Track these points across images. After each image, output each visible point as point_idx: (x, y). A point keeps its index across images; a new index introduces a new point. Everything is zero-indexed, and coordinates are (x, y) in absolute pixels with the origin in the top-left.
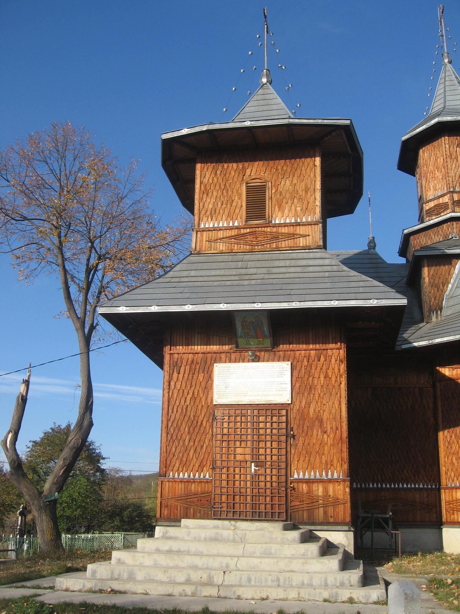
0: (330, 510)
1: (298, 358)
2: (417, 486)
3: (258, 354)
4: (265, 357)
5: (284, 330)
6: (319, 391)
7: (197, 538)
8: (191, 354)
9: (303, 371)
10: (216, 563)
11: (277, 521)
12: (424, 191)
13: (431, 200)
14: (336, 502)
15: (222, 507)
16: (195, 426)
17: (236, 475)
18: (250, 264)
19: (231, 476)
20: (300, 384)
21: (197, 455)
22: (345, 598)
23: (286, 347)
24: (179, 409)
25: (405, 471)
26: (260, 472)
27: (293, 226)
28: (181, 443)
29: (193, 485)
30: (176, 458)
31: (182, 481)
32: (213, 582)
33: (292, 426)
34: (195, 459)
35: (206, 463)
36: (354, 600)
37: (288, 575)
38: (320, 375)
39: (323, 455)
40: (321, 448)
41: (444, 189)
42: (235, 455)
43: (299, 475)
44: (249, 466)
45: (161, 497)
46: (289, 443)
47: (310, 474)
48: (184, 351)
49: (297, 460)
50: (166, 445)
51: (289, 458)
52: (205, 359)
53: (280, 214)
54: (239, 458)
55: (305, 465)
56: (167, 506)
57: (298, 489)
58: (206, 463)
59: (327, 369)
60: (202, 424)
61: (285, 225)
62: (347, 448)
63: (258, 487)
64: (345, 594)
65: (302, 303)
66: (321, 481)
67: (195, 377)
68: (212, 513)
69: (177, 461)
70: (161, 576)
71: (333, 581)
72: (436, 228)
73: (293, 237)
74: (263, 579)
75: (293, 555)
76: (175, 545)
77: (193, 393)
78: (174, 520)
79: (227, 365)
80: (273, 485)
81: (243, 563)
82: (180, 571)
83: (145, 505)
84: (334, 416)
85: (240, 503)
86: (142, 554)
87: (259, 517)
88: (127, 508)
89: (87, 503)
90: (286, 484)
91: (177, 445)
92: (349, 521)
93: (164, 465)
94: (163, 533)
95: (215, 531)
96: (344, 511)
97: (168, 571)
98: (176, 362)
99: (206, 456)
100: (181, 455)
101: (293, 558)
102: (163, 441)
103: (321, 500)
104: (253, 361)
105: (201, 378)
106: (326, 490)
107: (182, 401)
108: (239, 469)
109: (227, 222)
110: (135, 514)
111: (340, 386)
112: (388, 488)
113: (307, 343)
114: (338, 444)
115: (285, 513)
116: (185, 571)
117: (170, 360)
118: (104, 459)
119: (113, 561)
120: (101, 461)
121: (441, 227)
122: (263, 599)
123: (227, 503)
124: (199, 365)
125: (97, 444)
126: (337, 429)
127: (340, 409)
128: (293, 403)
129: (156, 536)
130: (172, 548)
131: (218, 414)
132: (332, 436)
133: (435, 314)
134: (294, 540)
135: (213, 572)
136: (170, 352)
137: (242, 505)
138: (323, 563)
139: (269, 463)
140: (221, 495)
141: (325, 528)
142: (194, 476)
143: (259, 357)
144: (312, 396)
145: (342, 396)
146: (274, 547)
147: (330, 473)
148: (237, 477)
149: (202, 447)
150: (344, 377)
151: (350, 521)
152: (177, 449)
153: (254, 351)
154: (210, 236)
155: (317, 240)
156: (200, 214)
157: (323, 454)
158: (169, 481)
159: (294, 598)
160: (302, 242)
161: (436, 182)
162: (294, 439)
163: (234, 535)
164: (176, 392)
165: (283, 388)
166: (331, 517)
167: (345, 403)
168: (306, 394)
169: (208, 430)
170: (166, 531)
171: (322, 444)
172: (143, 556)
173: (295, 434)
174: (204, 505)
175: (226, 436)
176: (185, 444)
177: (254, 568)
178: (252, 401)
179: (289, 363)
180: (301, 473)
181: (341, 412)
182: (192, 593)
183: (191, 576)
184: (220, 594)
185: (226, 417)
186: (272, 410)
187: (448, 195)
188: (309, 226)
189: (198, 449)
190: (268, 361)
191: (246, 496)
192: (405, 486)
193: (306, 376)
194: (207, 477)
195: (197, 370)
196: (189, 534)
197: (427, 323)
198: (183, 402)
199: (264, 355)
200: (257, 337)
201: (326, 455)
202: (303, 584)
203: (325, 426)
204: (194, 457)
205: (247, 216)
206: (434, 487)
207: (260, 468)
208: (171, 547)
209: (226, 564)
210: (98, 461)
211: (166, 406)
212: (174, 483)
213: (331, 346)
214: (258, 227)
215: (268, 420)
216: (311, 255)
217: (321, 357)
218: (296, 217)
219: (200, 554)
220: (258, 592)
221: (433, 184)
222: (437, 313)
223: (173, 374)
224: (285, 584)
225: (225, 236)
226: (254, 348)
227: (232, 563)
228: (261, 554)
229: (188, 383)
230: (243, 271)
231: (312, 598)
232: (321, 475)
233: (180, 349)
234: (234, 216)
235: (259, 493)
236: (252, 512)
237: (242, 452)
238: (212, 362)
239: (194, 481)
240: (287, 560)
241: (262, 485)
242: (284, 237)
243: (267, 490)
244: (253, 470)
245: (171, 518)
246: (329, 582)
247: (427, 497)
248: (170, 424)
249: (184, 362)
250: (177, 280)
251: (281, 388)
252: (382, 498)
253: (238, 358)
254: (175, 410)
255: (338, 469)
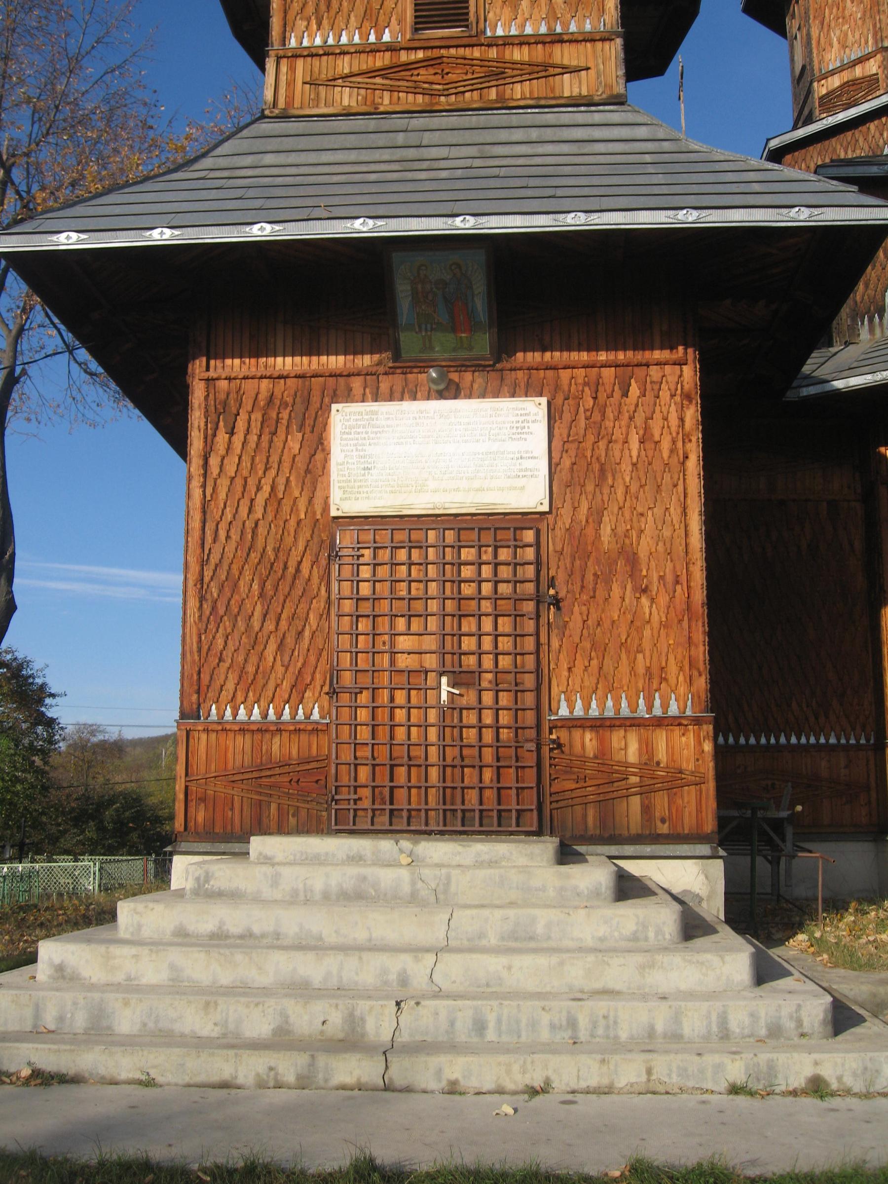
0: (661, 803)
1: (566, 388)
2: (822, 740)
3: (454, 376)
4: (476, 386)
5: (534, 302)
6: (628, 479)
7: (302, 894)
8: (265, 381)
9: (582, 423)
10: (366, 971)
11: (512, 833)
12: (815, 51)
13: (833, 73)
14: (675, 780)
15: (360, 799)
16: (278, 577)
17: (398, 711)
18: (427, 138)
19: (383, 713)
20: (575, 461)
21: (286, 659)
22: (798, 1081)
23: (533, 357)
24: (233, 531)
25: (794, 705)
26: (464, 702)
27: (544, 43)
28: (241, 625)
29: (277, 740)
30: (227, 665)
31: (244, 729)
32: (363, 1035)
33: (552, 573)
34: (280, 669)
35: (313, 679)
36: (827, 1084)
37: (602, 1006)
38: (627, 434)
39: (638, 652)
40: (634, 633)
41: (867, 42)
42: (393, 654)
43: (571, 709)
44: (434, 685)
45: (187, 775)
46: (543, 620)
47: (602, 706)
48: (245, 371)
49: (566, 666)
50: (199, 630)
51: (544, 662)
52: (306, 393)
53: (507, 12)
54: (403, 662)
55: (590, 682)
56: (203, 799)
57: (571, 746)
58: (313, 679)
59: (647, 419)
60: (298, 570)
61: (522, 39)
62: (704, 632)
63: (458, 743)
64: (797, 1068)
65: (595, 216)
66: (633, 723)
67: (278, 441)
68: (329, 816)
69: (230, 676)
70: (193, 1020)
71: (747, 1021)
72: (849, 134)
73: (543, 74)
74: (523, 1024)
75: (602, 940)
76: (233, 918)
77: (273, 488)
78: (228, 836)
79: (368, 409)
80: (501, 736)
81: (453, 970)
82: (257, 1005)
83: (150, 795)
84: (668, 545)
85: (409, 788)
86: (134, 950)
87: (463, 825)
88: (111, 801)
89: (17, 794)
90: (539, 733)
91: (229, 630)
92: (712, 832)
93: (192, 685)
94: (198, 879)
95: (353, 871)
96: (699, 805)
97: (216, 1003)
98: (225, 404)
99: (312, 659)
100: (241, 658)
101: (602, 950)
102: (190, 620)
103: (634, 774)
104: (441, 395)
105: (294, 445)
106: (647, 748)
107: (241, 508)
108: (404, 692)
109: (360, 34)
110: (127, 814)
111: (683, 463)
112: (753, 746)
113: (591, 347)
114: (680, 621)
115: (535, 813)
116: (271, 1002)
117: (207, 397)
118: (53, 696)
119: (42, 969)
120: (48, 701)
121: (863, 129)
122: (533, 1092)
123: (374, 788)
124: (289, 408)
125: (37, 665)
126: (677, 582)
127: (686, 526)
128: (554, 511)
129: (175, 884)
130: (225, 928)
131: (344, 540)
132: (663, 600)
133: (866, 322)
134: (596, 894)
135: (363, 1006)
136: (206, 375)
137: (413, 791)
138: (702, 963)
139: (489, 676)
140: (356, 765)
141: (648, 849)
142: (279, 715)
143: (458, 385)
144: (606, 491)
145: (689, 491)
146: (543, 919)
147: (657, 702)
148: (400, 715)
149: (300, 633)
150: (694, 439)
151: (716, 829)
152: (230, 642)
153: (444, 370)
154: (316, 70)
155: (609, 81)
156: (285, 12)
157: (640, 650)
158: (207, 731)
159: (632, 1085)
160: (569, 86)
161: (846, 27)
162: (559, 609)
163: (413, 883)
164: (224, 483)
165: (526, 470)
166: (663, 821)
167: (697, 510)
168: (590, 487)
169: (315, 587)
170: (207, 873)
171: (636, 623)
172: (134, 956)
173: (562, 594)
174: (305, 794)
175: (369, 604)
176: (252, 627)
177: (488, 985)
178: (447, 505)
179: (544, 400)
180: (579, 704)
181: (686, 535)
182: (299, 1077)
183: (292, 1020)
184: (391, 1079)
185: (366, 552)
186: (496, 529)
187: (879, 56)
188: (588, 45)
189: (290, 640)
190: (483, 396)
191: (427, 766)
192: (794, 740)
193: (591, 438)
194: (316, 716)
195: (285, 422)
196: (275, 882)
197: (847, 344)
198: (244, 511)
199: (473, 381)
200: (454, 330)
201: (648, 653)
202: (651, 1033)
203: (644, 573)
204: (279, 662)
205: (416, 17)
206: (863, 741)
207: (463, 691)
208: (222, 923)
209: (399, 975)
210: (40, 701)
211: (196, 524)
212: (222, 736)
213: (657, 355)
214: (449, 47)
215: (484, 558)
216: (597, 118)
217: (630, 385)
218: (552, 22)
219: (313, 946)
220: (516, 1068)
221: (838, 32)
222: (871, 321)
223: (214, 435)
224: (592, 1036)
225: (355, 69)
226: (444, 360)
227: (419, 970)
228: (503, 939)
229: (257, 459)
230: (411, 153)
231: (691, 1084)
232: (634, 707)
233: (234, 365)
234: (381, 18)
235: (463, 759)
236: (445, 811)
237: (414, 646)
238: (326, 400)
239: (279, 729)
240: (591, 958)
241: (471, 735)
242: (519, 72)
243: (483, 749)
244: (444, 696)
245: (217, 830)
246: (734, 1026)
247: (846, 767)
248: (208, 574)
249: (248, 404)
250: (226, 174)
251: (521, 470)
252: (739, 771)
253: (398, 388)
254: (222, 534)
255: (682, 689)
